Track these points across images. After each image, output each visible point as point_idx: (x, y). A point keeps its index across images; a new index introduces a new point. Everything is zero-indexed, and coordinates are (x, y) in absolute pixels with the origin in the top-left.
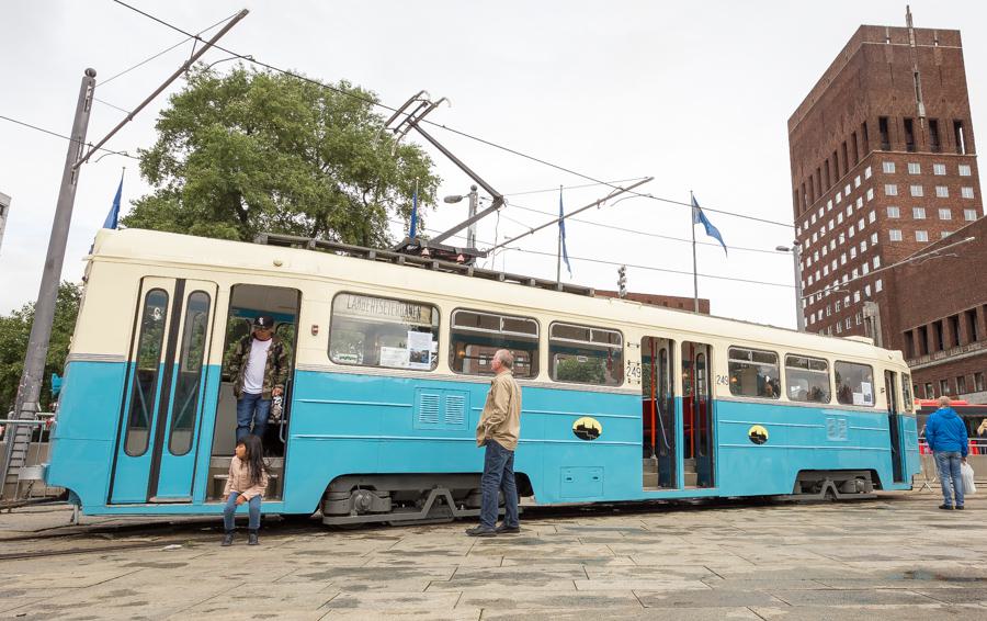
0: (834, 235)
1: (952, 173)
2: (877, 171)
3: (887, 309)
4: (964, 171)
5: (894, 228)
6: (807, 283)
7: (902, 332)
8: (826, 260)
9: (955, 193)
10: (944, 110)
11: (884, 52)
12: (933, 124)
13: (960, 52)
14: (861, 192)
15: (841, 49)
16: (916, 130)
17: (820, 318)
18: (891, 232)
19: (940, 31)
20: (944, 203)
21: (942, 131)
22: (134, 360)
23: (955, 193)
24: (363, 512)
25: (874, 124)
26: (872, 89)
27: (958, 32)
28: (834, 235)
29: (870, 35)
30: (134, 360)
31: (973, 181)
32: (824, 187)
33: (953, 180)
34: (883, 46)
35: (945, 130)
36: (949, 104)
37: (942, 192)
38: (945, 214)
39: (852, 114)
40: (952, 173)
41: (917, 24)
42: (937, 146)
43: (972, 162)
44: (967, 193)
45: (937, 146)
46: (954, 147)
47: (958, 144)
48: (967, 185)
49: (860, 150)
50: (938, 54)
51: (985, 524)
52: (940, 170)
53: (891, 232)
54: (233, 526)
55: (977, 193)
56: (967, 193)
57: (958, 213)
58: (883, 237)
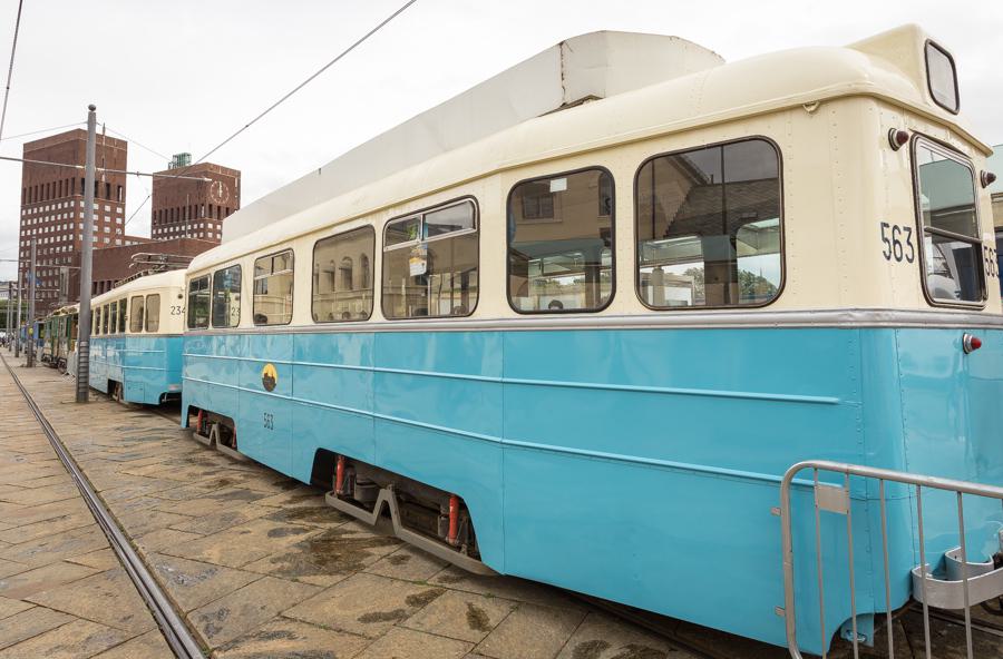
0: (55, 223)
4: (119, 210)
8: (38, 226)
9: (113, 220)
10: (114, 180)
12: (108, 185)
16: (100, 188)
19: (119, 140)
20: (108, 225)
21: (112, 189)
22: (344, 536)
23: (113, 220)
24: (122, 637)
28: (55, 223)
30: (344, 536)
31: (122, 216)
33: (113, 214)
35: (113, 189)
37: (107, 219)
38: (108, 208)
41: (108, 134)
42: (108, 197)
43: (123, 207)
44: (119, 221)
45: (108, 197)
51: (999, 490)
52: (108, 208)
54: (357, 317)
56: (119, 221)
58: (76, 237)
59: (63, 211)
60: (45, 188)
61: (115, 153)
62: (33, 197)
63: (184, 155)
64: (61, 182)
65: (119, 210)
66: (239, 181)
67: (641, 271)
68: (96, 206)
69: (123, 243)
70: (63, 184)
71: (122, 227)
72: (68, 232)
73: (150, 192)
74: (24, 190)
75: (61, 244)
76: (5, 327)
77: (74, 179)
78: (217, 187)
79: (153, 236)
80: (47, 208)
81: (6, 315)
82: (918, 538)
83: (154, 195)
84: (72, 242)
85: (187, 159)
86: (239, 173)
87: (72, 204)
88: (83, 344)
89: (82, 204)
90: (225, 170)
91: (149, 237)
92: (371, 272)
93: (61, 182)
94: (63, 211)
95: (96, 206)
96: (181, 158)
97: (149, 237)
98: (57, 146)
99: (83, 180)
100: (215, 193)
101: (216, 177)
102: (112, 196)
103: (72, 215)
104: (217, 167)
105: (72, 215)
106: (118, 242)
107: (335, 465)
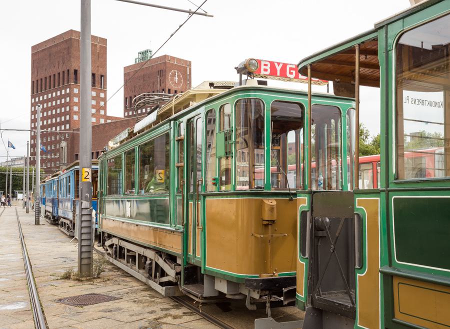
0: (55, 108)
1: (98, 95)
2: (71, 90)
3: (70, 145)
4: (102, 95)
5: (75, 115)
6: (43, 123)
7: (74, 154)
9: (98, 103)
10: (98, 71)
11: (79, 42)
13: (106, 48)
14: (65, 96)
15: (66, 31)
17: (59, 118)
18: (74, 116)
23: (98, 103)
25: (72, 72)
26: (73, 58)
27: (125, 68)
28: (55, 108)
29: (74, 35)
31: (105, 100)
32: (57, 84)
34: (78, 40)
35: (97, 78)
36: (100, 68)
39: (64, 63)
40: (98, 95)
41: (424, 47)
44: (102, 104)
46: (100, 85)
47: (101, 85)
48: (102, 109)
49: (66, 80)
50: (98, 47)
53: (74, 116)
55: (105, 104)
56: (102, 104)
57: (98, 111)
59: (60, 97)
60: (48, 80)
61: (100, 48)
62: (39, 87)
63: (147, 51)
64: (59, 74)
65: (102, 95)
66: (190, 69)
67: (360, 157)
68: (94, 94)
69: (106, 121)
70: (61, 76)
71: (105, 108)
72: (65, 114)
73: (123, 83)
74: (33, 82)
75: (56, 125)
76: (22, 189)
77: (68, 71)
78: (174, 75)
79: (125, 116)
80: (50, 96)
81: (23, 177)
82: (221, 116)
83: (125, 85)
84: (68, 122)
85: (149, 54)
86: (190, 62)
87: (68, 91)
88: (329, 160)
89: (76, 91)
90: (179, 60)
91: (123, 117)
92: (262, 108)
93: (59, 74)
94: (60, 97)
95: (94, 94)
96: (144, 53)
97: (123, 117)
98: (56, 46)
99: (76, 72)
100: (172, 80)
101: (174, 66)
102: (96, 84)
103: (68, 100)
104: (173, 58)
105: (68, 100)
106: (102, 121)
107: (265, 307)
